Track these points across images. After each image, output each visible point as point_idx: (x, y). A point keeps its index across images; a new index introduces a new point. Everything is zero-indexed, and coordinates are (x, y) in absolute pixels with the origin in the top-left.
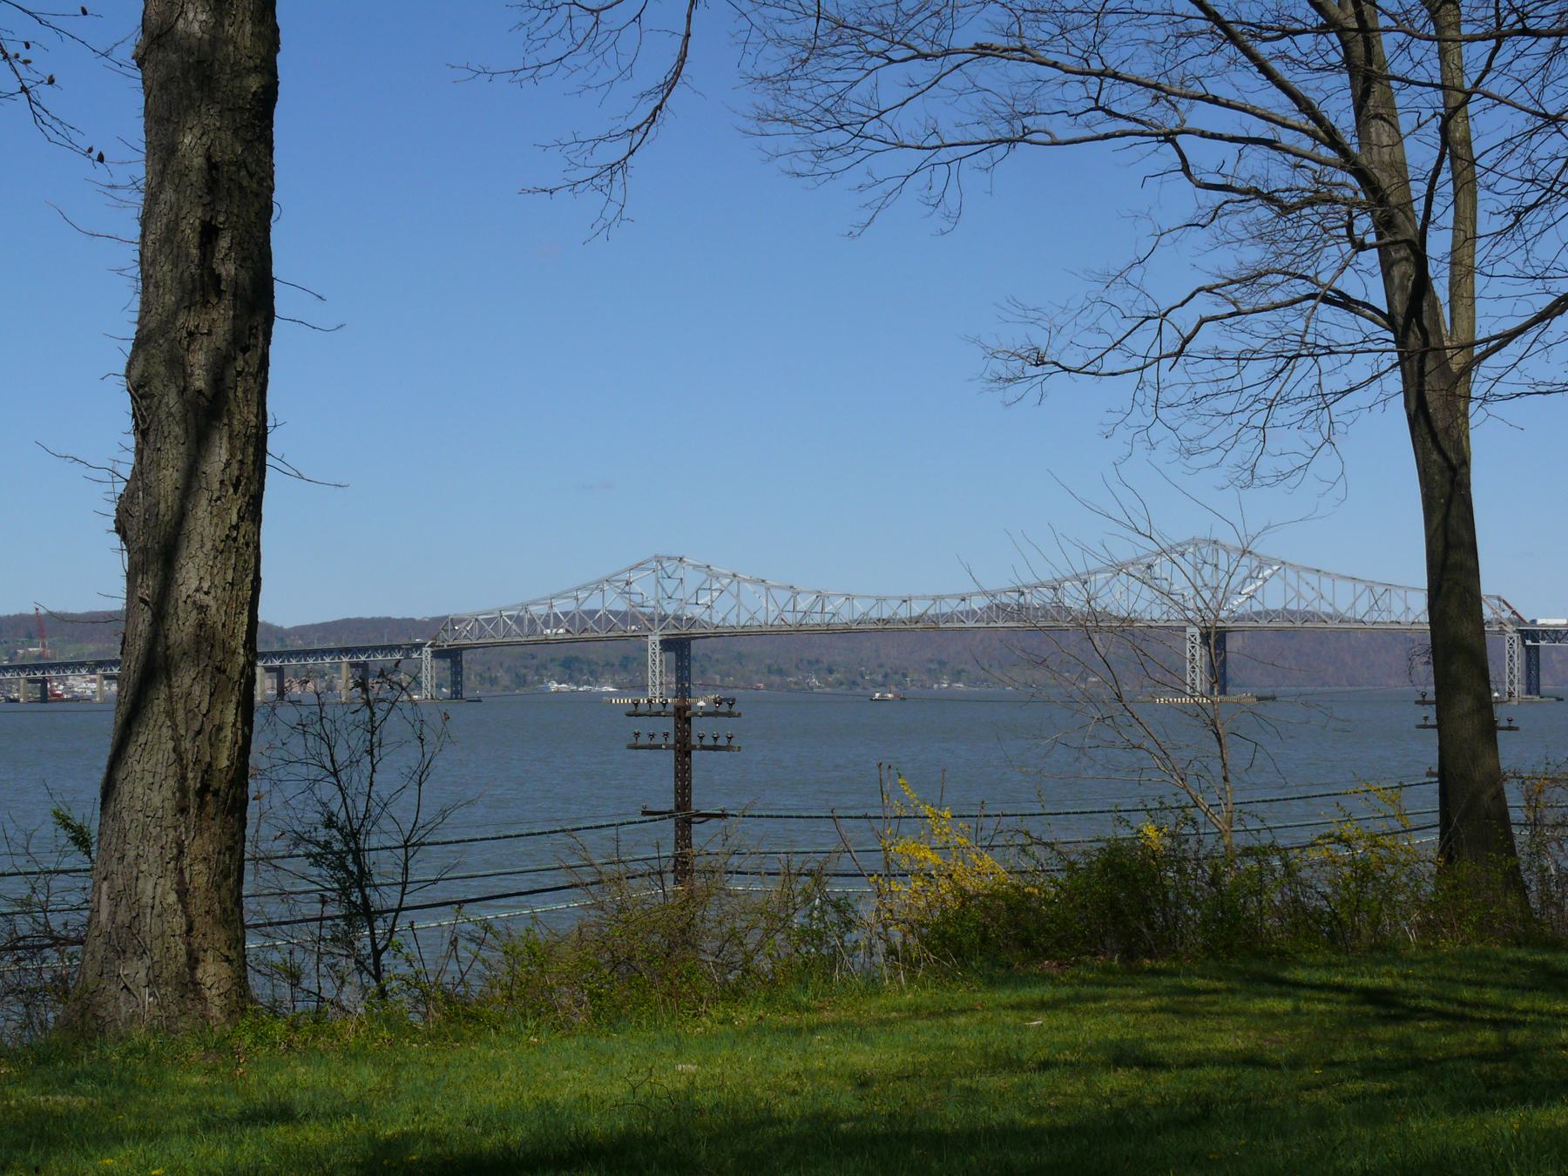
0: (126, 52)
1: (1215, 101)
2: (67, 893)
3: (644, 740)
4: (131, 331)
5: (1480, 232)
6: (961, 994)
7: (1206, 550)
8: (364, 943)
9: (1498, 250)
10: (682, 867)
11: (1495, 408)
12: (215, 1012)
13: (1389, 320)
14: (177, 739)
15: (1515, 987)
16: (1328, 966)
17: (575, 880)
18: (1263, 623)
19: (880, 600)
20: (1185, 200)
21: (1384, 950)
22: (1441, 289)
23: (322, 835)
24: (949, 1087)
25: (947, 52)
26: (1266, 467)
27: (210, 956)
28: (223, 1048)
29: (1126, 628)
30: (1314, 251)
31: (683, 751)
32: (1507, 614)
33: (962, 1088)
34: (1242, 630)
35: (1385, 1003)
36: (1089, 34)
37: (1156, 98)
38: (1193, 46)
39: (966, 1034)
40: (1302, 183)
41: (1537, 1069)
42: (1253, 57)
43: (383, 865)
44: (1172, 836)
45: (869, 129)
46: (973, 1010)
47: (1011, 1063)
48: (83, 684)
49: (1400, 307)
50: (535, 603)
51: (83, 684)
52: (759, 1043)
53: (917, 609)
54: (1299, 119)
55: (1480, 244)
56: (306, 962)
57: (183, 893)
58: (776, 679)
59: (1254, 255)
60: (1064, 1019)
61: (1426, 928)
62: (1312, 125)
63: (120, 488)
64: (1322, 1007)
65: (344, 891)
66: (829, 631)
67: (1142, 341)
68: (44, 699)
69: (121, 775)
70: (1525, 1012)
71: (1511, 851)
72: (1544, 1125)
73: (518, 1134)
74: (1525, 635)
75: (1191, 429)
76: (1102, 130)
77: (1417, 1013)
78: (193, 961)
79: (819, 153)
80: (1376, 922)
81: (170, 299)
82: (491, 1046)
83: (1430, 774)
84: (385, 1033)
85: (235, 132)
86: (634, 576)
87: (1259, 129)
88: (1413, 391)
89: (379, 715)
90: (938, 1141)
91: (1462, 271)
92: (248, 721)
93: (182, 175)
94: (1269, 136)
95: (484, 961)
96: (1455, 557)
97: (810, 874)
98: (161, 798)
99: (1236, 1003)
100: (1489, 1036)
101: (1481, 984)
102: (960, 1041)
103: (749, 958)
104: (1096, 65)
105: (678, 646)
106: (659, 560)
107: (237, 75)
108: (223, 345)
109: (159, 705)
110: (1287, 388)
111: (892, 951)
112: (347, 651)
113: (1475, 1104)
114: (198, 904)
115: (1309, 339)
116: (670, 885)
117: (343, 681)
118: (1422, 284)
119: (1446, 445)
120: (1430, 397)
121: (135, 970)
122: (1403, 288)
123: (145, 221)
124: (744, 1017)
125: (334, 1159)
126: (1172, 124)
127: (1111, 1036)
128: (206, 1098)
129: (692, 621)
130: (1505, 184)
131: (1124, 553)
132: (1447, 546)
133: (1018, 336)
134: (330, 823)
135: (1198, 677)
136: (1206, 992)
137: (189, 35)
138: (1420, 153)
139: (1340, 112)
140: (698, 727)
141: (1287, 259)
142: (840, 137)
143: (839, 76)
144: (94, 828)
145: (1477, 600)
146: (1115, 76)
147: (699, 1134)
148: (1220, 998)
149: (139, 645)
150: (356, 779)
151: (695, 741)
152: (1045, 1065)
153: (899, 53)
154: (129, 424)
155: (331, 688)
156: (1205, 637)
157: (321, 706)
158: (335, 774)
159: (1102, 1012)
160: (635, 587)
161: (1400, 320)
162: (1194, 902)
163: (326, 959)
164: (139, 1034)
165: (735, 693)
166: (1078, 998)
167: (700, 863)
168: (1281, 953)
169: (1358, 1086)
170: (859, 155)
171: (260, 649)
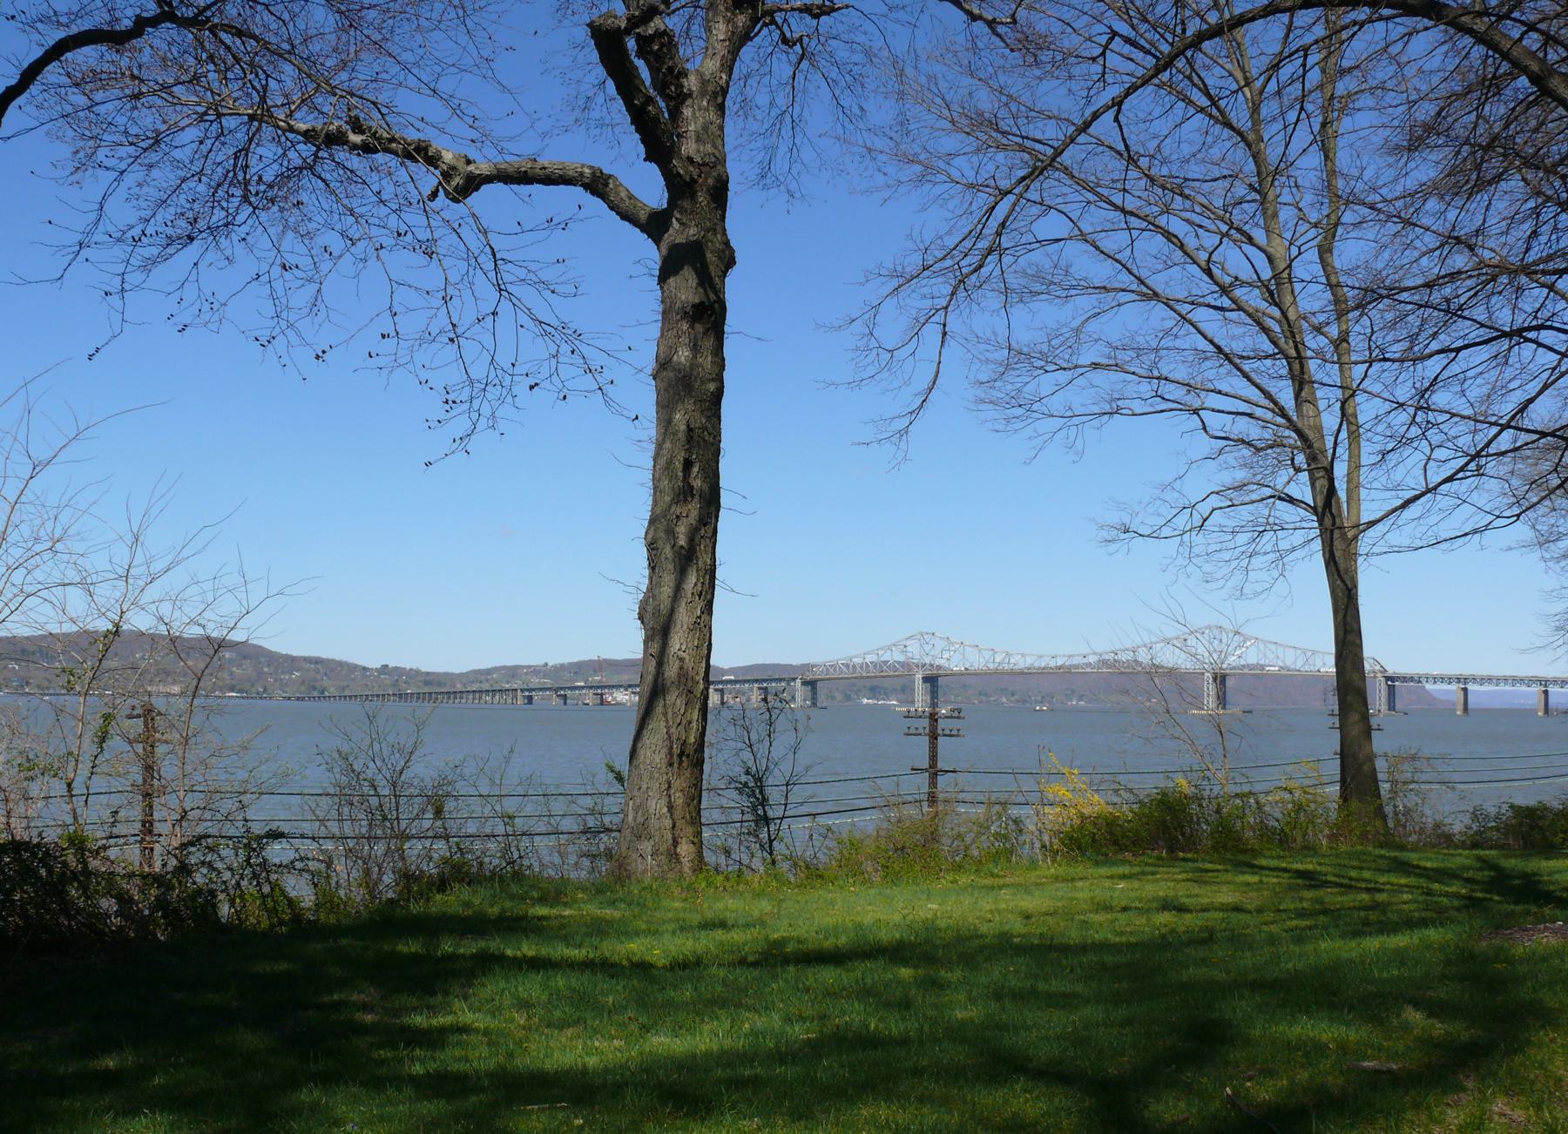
0: (649, 370)
1: (1220, 392)
2: (612, 804)
3: (912, 731)
4: (647, 516)
5: (1363, 463)
6: (1080, 870)
7: (1216, 632)
8: (764, 835)
9: (1373, 474)
10: (932, 799)
11: (1374, 560)
12: (686, 869)
13: (1314, 510)
14: (668, 727)
15: (1379, 870)
16: (1279, 857)
17: (875, 804)
18: (1246, 671)
19: (1040, 657)
20: (1204, 445)
21: (1310, 849)
22: (1342, 494)
23: (744, 778)
24: (1072, 919)
25: (1076, 367)
26: (1248, 589)
27: (684, 841)
28: (690, 888)
29: (1171, 673)
30: (1273, 473)
31: (934, 737)
32: (1378, 667)
33: (1080, 921)
34: (1234, 675)
35: (1310, 879)
36: (1152, 357)
37: (1189, 391)
38: (1208, 364)
39: (1083, 892)
40: (1267, 437)
41: (1390, 915)
42: (1239, 369)
43: (774, 795)
44: (1196, 786)
45: (1035, 407)
46: (1086, 878)
47: (1108, 908)
48: (621, 696)
49: (1320, 503)
50: (868, 653)
51: (621, 696)
52: (972, 894)
53: (1060, 662)
54: (1266, 402)
55: (1363, 470)
56: (733, 844)
57: (671, 808)
58: (983, 698)
59: (1241, 475)
60: (1136, 884)
61: (1333, 837)
62: (1272, 406)
63: (641, 596)
64: (1275, 880)
65: (754, 808)
66: (1012, 673)
67: (1182, 521)
68: (602, 704)
69: (640, 745)
70: (1384, 884)
71: (1379, 796)
72: (1393, 946)
73: (843, 940)
74: (1388, 678)
75: (1208, 568)
76: (1159, 408)
77: (1326, 884)
78: (675, 843)
79: (1008, 420)
80: (1305, 835)
81: (667, 499)
82: (830, 891)
83: (1336, 754)
84: (774, 884)
85: (702, 412)
86: (908, 643)
87: (1244, 407)
88: (1327, 549)
89: (774, 717)
90: (1065, 949)
91: (1353, 486)
92: (704, 718)
93: (675, 434)
94: (1249, 411)
95: (827, 847)
96: (1350, 638)
97: (1001, 803)
98: (659, 759)
99: (1229, 877)
100: (1365, 897)
101: (1361, 869)
102: (1080, 895)
103: (967, 848)
104: (1156, 374)
105: (931, 680)
106: (922, 635)
107: (703, 382)
108: (694, 523)
109: (659, 709)
110: (1258, 548)
111: (1044, 846)
112: (756, 681)
113: (1356, 934)
114: (678, 813)
115: (1271, 520)
116: (926, 809)
117: (756, 697)
118: (1331, 491)
119: (1345, 577)
120: (1338, 554)
121: (646, 847)
122: (1322, 492)
123: (655, 460)
124: (964, 880)
125: (746, 949)
126: (1197, 405)
127: (1161, 894)
128: (681, 915)
129: (939, 667)
130: (1377, 438)
131: (1170, 634)
132: (1346, 632)
133: (1115, 518)
134: (747, 773)
135: (1210, 701)
136: (1213, 871)
137: (680, 363)
138: (1330, 420)
139: (1286, 396)
140: (941, 724)
141: (1259, 477)
142: (1020, 411)
143: (1019, 379)
144: (625, 774)
145: (1361, 659)
146: (1166, 379)
147: (938, 942)
148: (1220, 874)
149: (650, 679)
150: (762, 750)
151: (940, 732)
152: (1125, 909)
153: (1051, 367)
154: (646, 563)
155: (749, 700)
156: (1215, 679)
157: (744, 710)
158: (751, 746)
159: (1157, 881)
160: (909, 649)
161: (1320, 510)
162: (1207, 823)
163: (745, 843)
164: (647, 880)
165: (962, 706)
166: (1143, 873)
167: (941, 796)
168: (1253, 850)
169: (1294, 923)
170: (1029, 421)
171: (711, 679)
